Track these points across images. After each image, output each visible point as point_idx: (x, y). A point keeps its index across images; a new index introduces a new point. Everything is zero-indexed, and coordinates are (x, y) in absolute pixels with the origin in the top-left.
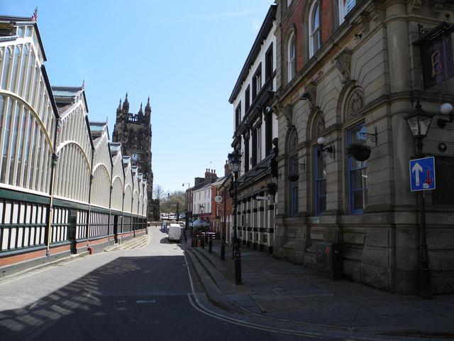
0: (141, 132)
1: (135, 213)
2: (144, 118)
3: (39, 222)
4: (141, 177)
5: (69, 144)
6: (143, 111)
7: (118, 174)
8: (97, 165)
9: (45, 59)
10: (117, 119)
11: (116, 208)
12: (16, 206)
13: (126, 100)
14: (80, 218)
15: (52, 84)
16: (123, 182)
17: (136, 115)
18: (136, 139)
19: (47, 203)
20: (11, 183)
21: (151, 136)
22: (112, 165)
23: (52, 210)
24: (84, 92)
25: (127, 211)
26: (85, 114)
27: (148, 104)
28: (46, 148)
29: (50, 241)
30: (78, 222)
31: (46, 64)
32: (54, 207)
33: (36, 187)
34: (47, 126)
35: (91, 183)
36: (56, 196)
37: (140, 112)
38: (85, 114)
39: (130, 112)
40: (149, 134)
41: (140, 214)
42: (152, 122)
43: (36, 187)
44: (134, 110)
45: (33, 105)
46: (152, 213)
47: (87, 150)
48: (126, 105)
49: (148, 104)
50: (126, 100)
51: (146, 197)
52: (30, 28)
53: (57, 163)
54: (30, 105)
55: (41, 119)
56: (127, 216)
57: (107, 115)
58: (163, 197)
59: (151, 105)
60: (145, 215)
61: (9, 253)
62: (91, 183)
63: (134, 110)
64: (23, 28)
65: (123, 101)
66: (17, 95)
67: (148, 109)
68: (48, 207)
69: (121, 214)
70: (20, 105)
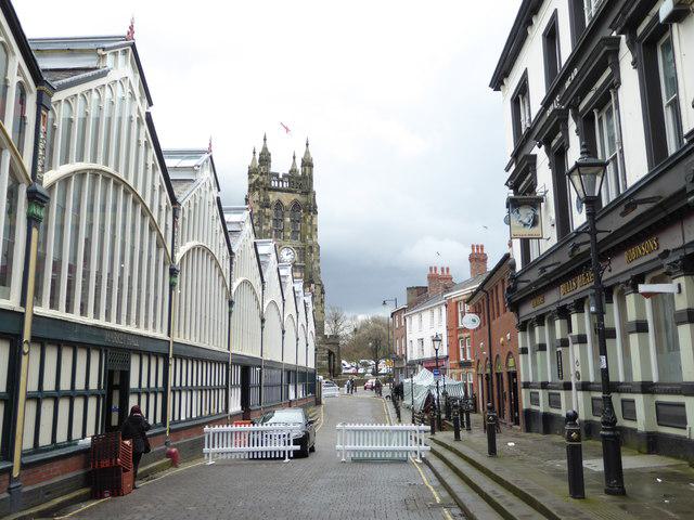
0: (296, 205)
1: (290, 360)
2: (301, 181)
3: (152, 385)
4: (299, 286)
5: (81, 175)
6: (299, 167)
7: (273, 292)
8: (189, 245)
9: (150, 103)
10: (250, 186)
11: (245, 348)
12: (51, 356)
13: (265, 149)
14: (139, 373)
15: (164, 147)
16: (281, 308)
17: (284, 176)
18: (288, 220)
19: (164, 350)
20: (53, 305)
22: (231, 252)
23: (172, 362)
24: (211, 157)
25: (272, 354)
26: (215, 193)
27: (307, 152)
28: (158, 255)
29: (169, 419)
30: (134, 384)
31: (151, 110)
32: (40, 341)
33: (154, 327)
34: (159, 219)
35: (230, 313)
36: (177, 340)
37: (293, 171)
38: (215, 193)
39: (273, 169)
40: (312, 209)
41: (302, 363)
42: (316, 187)
43: (154, 327)
44: (281, 165)
45: (127, 177)
46: (325, 362)
47: (221, 253)
48: (265, 158)
49: (307, 152)
50: (265, 149)
51: (312, 327)
52: (125, 52)
53: (266, 324)
54: (132, 184)
55: (148, 206)
56: (271, 365)
57: (236, 185)
58: (346, 331)
59: (312, 155)
60: (311, 365)
61: (218, 417)
62: (262, 328)
63: (281, 165)
64: (115, 54)
65: (259, 151)
66: (110, 169)
67: (307, 164)
68: (166, 357)
69: (258, 363)
70: (116, 185)
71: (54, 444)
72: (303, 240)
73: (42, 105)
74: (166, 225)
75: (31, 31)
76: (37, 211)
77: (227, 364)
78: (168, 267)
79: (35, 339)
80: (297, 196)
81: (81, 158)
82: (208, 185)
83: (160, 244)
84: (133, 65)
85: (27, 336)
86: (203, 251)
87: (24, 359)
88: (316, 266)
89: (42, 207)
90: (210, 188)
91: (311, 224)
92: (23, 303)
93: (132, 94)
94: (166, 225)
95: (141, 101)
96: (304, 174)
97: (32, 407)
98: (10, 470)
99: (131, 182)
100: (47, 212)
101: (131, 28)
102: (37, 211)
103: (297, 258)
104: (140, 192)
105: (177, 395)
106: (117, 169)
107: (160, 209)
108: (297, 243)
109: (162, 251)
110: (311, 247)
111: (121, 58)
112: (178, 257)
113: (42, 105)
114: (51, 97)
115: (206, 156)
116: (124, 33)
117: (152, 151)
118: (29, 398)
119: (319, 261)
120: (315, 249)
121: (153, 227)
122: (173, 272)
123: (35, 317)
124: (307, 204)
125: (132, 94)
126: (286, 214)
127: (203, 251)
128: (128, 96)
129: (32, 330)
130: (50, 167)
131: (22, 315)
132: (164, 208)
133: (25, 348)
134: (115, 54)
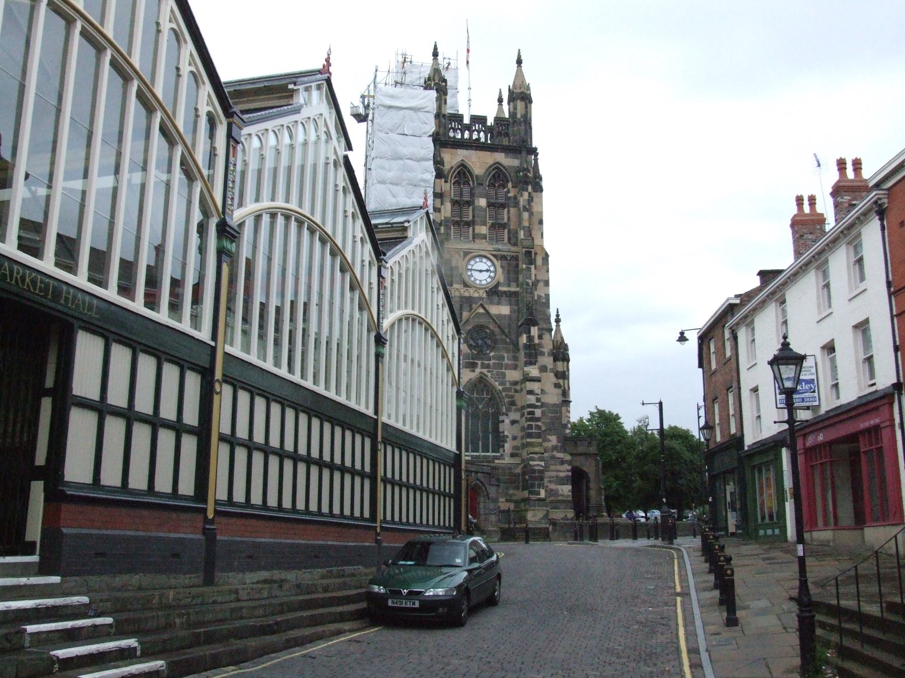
0: (498, 175)
18: (483, 202)
21: (538, 188)
23: (381, 447)
27: (519, 75)
29: (380, 516)
31: (349, 153)
35: (379, 356)
45: (312, 213)
49: (519, 75)
52: (319, 87)
54: (329, 232)
55: (340, 245)
66: (293, 205)
70: (300, 223)
71: (320, 512)
72: (513, 240)
73: (232, 139)
74: (370, 283)
75: (226, 75)
76: (227, 244)
77: (206, 374)
78: (373, 334)
79: (227, 379)
80: (500, 157)
81: (406, 308)
82: (424, 250)
83: (363, 305)
84: (329, 103)
85: (218, 375)
86: (414, 320)
87: (216, 398)
88: (540, 292)
89: (232, 242)
90: (427, 253)
91: (528, 209)
92: (214, 337)
93: (328, 133)
94: (370, 283)
95: (339, 142)
96: (513, 114)
97: (224, 449)
98: (204, 511)
99: (429, 321)
100: (238, 247)
101: (328, 60)
102: (227, 244)
103: (501, 277)
104: (339, 242)
105: (389, 487)
106: (420, 312)
107: (363, 266)
108: (505, 247)
109: (365, 315)
110: (528, 253)
111: (315, 94)
112: (386, 324)
113: (232, 139)
114: (241, 129)
115: (423, 211)
116: (319, 65)
117: (351, 197)
118: (222, 438)
119: (547, 283)
120: (539, 261)
121: (355, 286)
122: (380, 341)
123: (227, 355)
124: (518, 170)
125: (328, 133)
126: (478, 191)
127: (414, 320)
128: (323, 137)
129: (224, 368)
130: (240, 205)
131: (213, 350)
132: (366, 263)
133: (217, 387)
134: (307, 89)
